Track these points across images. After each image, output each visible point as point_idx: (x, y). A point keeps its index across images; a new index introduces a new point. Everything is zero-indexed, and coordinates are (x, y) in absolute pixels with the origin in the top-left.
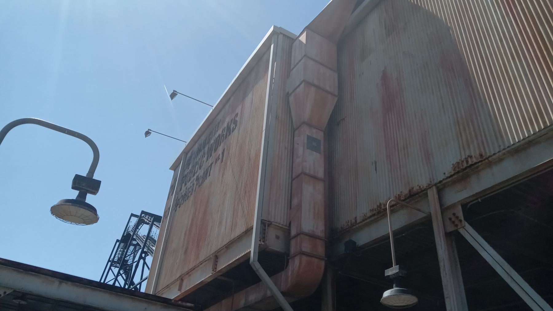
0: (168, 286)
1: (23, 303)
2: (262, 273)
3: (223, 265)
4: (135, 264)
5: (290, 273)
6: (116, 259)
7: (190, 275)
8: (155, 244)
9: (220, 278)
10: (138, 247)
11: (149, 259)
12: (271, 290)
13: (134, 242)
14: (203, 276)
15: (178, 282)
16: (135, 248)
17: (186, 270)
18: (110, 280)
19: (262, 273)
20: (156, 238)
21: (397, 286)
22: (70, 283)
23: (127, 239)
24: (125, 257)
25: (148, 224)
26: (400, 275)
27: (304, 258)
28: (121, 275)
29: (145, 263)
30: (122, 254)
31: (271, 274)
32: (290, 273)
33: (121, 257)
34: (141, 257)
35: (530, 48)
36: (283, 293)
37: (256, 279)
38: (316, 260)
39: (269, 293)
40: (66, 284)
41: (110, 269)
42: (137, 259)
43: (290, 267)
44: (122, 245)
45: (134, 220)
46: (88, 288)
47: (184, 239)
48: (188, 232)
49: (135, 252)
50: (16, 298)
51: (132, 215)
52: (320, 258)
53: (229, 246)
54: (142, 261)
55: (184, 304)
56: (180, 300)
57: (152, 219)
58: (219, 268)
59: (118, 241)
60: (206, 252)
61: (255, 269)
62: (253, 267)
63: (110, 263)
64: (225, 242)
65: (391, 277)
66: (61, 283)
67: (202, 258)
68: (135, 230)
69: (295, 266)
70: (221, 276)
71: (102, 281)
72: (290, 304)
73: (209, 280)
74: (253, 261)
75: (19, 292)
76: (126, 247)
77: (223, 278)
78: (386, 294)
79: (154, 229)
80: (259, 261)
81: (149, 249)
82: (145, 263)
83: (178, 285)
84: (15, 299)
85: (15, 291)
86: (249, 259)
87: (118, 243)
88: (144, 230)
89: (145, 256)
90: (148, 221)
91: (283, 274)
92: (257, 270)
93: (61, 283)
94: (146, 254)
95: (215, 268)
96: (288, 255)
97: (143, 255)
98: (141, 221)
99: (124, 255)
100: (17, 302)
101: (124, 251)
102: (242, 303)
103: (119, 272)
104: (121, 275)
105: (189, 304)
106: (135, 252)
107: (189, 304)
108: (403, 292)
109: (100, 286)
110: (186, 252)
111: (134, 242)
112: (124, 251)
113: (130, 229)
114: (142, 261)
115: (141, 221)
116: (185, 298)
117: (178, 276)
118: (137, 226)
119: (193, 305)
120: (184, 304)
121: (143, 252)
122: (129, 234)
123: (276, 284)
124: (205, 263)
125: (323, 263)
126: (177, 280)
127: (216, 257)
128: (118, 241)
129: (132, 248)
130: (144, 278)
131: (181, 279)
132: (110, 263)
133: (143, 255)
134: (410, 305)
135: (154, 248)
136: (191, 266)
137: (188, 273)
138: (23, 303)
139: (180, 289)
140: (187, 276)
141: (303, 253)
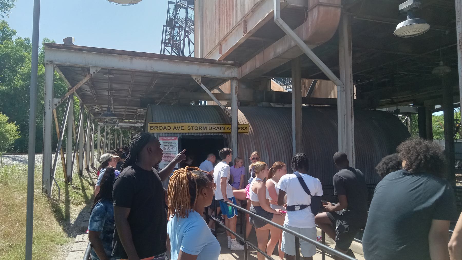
0: (211, 52)
1: (111, 76)
2: (286, 28)
3: (251, 27)
4: (182, 42)
5: (310, 24)
6: (167, 41)
7: (227, 40)
8: (193, 24)
9: (251, 38)
10: (181, 29)
11: (192, 36)
12: (295, 41)
13: (177, 25)
14: (237, 38)
15: (218, 47)
16: (179, 29)
17: (222, 37)
18: (166, 53)
19: (286, 28)
20: (193, 19)
21: (410, 18)
22: (138, 58)
23: (171, 23)
24: (173, 38)
25: (184, 8)
26: (414, 7)
27: (322, 8)
28: (174, 52)
29: (189, 40)
30: (171, 36)
31: (293, 28)
32: (310, 24)
33: (170, 38)
34: (185, 36)
35: (319, 105)
36: (305, 42)
37: (281, 34)
38: (332, 9)
39: (293, 44)
40: (136, 58)
41: (165, 48)
42: (182, 38)
43: (310, 19)
44: (168, 28)
45: (172, 7)
46: (151, 59)
47: (216, 12)
48: (217, 5)
49: (179, 32)
50: (105, 73)
51: (170, 2)
52: (336, 6)
53: (254, 10)
54: (187, 39)
55: (226, 62)
56: (223, 60)
57: (186, 3)
58: (249, 30)
59: (164, 26)
60: (236, 19)
61: (279, 25)
62: (277, 23)
63: (163, 44)
64: (251, 6)
65: (404, 10)
66: (132, 58)
67: (233, 24)
68: (175, 15)
69: (314, 17)
70: (251, 36)
71: (162, 53)
72: (312, 50)
73: (243, 41)
74: (277, 18)
75: (106, 69)
76: (172, 30)
77: (253, 38)
78: (400, 26)
79: (190, 11)
80: (281, 17)
81: (189, 28)
82: (189, 40)
83: (219, 50)
84: (105, 74)
85: (102, 69)
86: (273, 18)
87: (165, 28)
88: (182, 14)
89: (189, 34)
90: (183, 6)
91: (304, 25)
92: (281, 25)
93: (132, 58)
94: (188, 32)
95: (245, 31)
96: (307, 9)
97: (187, 34)
98: (178, 7)
99: (172, 36)
100: (107, 76)
101: (171, 33)
102: (272, 55)
103: (172, 50)
104: (174, 52)
105: (230, 62)
106: (180, 32)
107: (230, 62)
108: (416, 21)
109: (161, 57)
110: (219, 23)
111: (177, 25)
112: (171, 33)
113: (171, 15)
114: (187, 39)
115: (178, 7)
116: (227, 57)
117: (217, 43)
118: (176, 11)
119: (233, 62)
120: (226, 62)
121: (186, 31)
122: (171, 19)
123: (298, 35)
124: (236, 29)
125: (339, 11)
126: (217, 46)
127: (245, 21)
128: (164, 26)
129: (176, 30)
130: (191, 52)
131: (220, 44)
132: (163, 44)
133: (187, 34)
134: (423, 32)
135: (193, 27)
136: (226, 33)
137: (225, 39)
138: (111, 76)
139: (220, 53)
140: (224, 41)
141: (321, 4)
